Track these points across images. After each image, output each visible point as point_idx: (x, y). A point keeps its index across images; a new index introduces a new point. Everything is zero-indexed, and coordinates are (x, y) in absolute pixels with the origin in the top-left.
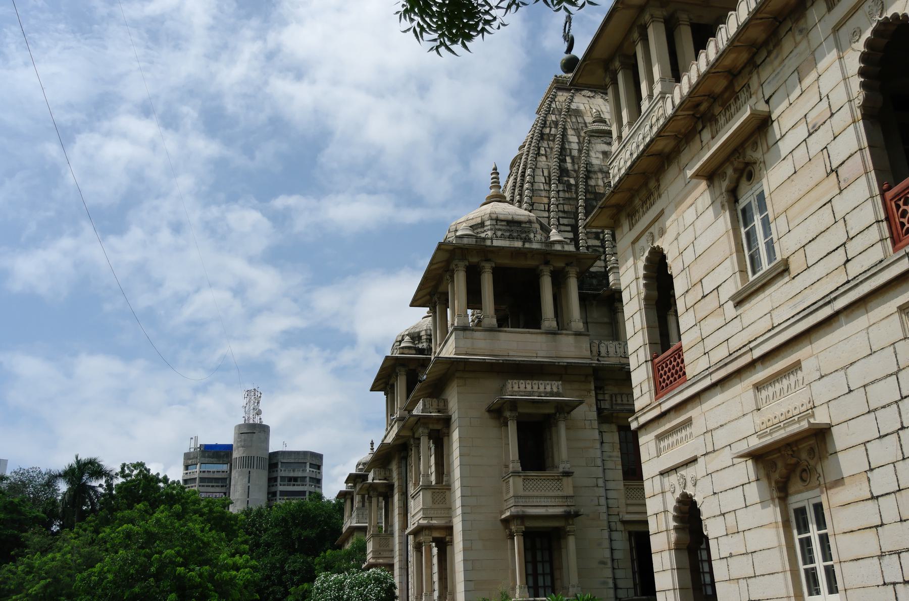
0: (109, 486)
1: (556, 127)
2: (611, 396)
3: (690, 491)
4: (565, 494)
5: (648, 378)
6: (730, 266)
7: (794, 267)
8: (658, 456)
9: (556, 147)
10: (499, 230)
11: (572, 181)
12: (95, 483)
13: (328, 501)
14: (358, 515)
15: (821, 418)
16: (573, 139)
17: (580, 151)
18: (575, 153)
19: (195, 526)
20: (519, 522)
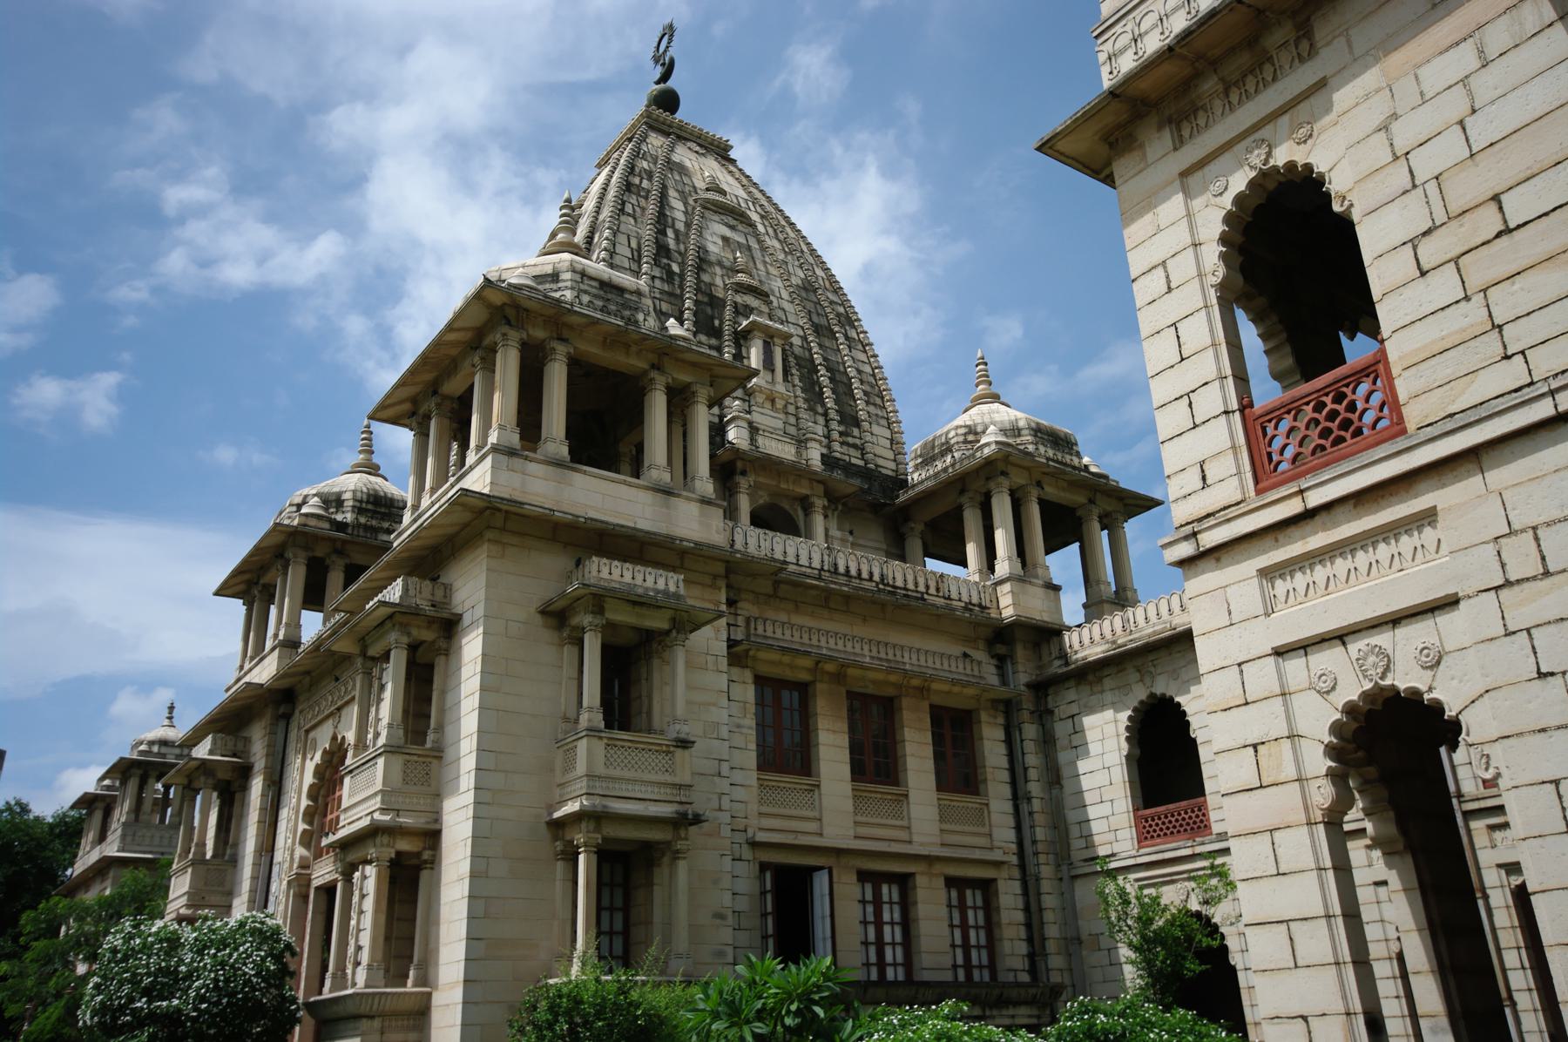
1: (650, 178)
2: (748, 621)
4: (677, 780)
5: (1234, 447)
8: (1267, 615)
9: (651, 208)
10: (586, 292)
11: (675, 268)
13: (37, 818)
14: (123, 837)
16: (678, 205)
17: (688, 225)
18: (681, 226)
20: (592, 826)
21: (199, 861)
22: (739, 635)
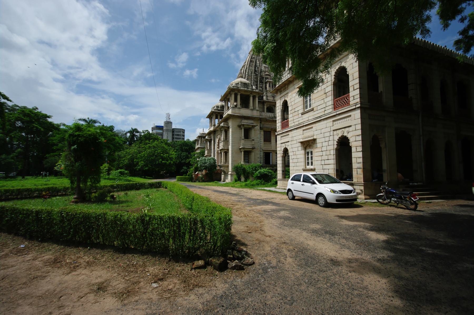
0: (140, 135)
3: (287, 147)
6: (301, 107)
7: (315, 109)
9: (254, 64)
12: (137, 134)
15: (315, 137)
16: (258, 62)
19: (163, 145)
21: (208, 149)
22: (262, 126)
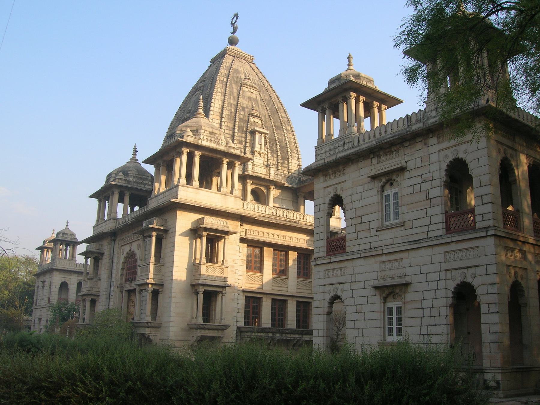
7: (408, 224)
